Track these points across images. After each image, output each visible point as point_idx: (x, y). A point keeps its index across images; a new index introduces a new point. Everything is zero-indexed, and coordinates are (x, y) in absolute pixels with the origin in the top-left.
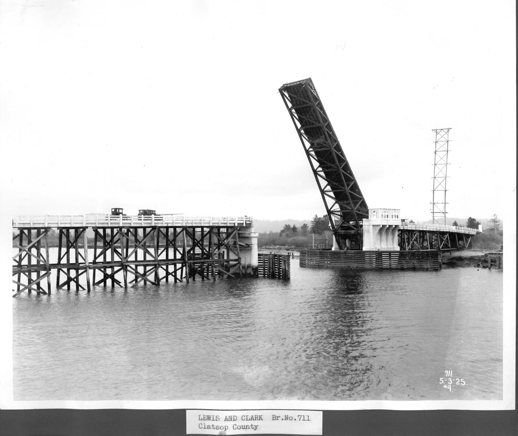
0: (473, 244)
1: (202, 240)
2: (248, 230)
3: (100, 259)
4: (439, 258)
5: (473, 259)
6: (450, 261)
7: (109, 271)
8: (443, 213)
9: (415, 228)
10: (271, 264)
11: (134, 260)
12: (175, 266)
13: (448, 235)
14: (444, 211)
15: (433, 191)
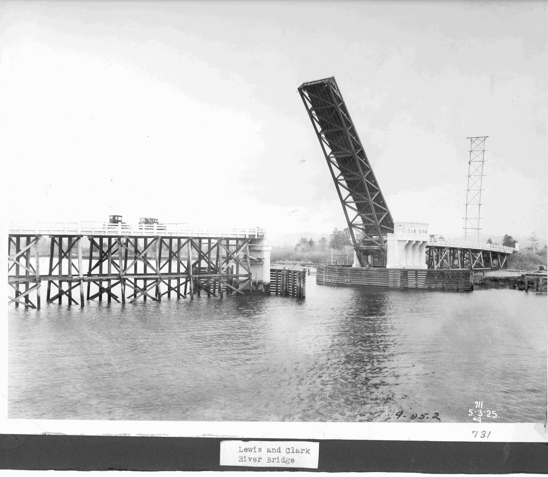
0: (509, 264)
1: (209, 252)
2: (261, 242)
5: (508, 280)
6: (483, 282)
11: (98, 273)
12: (179, 281)
13: (481, 253)
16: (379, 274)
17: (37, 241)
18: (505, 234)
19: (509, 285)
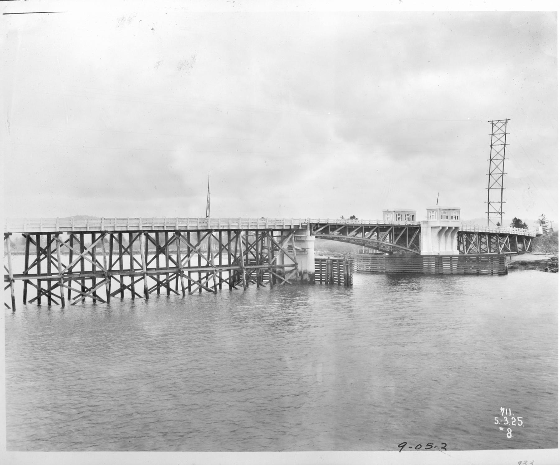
0: (533, 248)
1: (229, 244)
2: (304, 233)
3: (153, 265)
4: (505, 263)
5: (538, 263)
6: (512, 265)
7: (162, 278)
8: (499, 213)
9: (474, 230)
10: (330, 270)
12: (200, 275)
13: (508, 237)
14: (500, 212)
15: (488, 190)
16: (414, 261)
17: (103, 237)
18: (514, 218)
19: (540, 268)
